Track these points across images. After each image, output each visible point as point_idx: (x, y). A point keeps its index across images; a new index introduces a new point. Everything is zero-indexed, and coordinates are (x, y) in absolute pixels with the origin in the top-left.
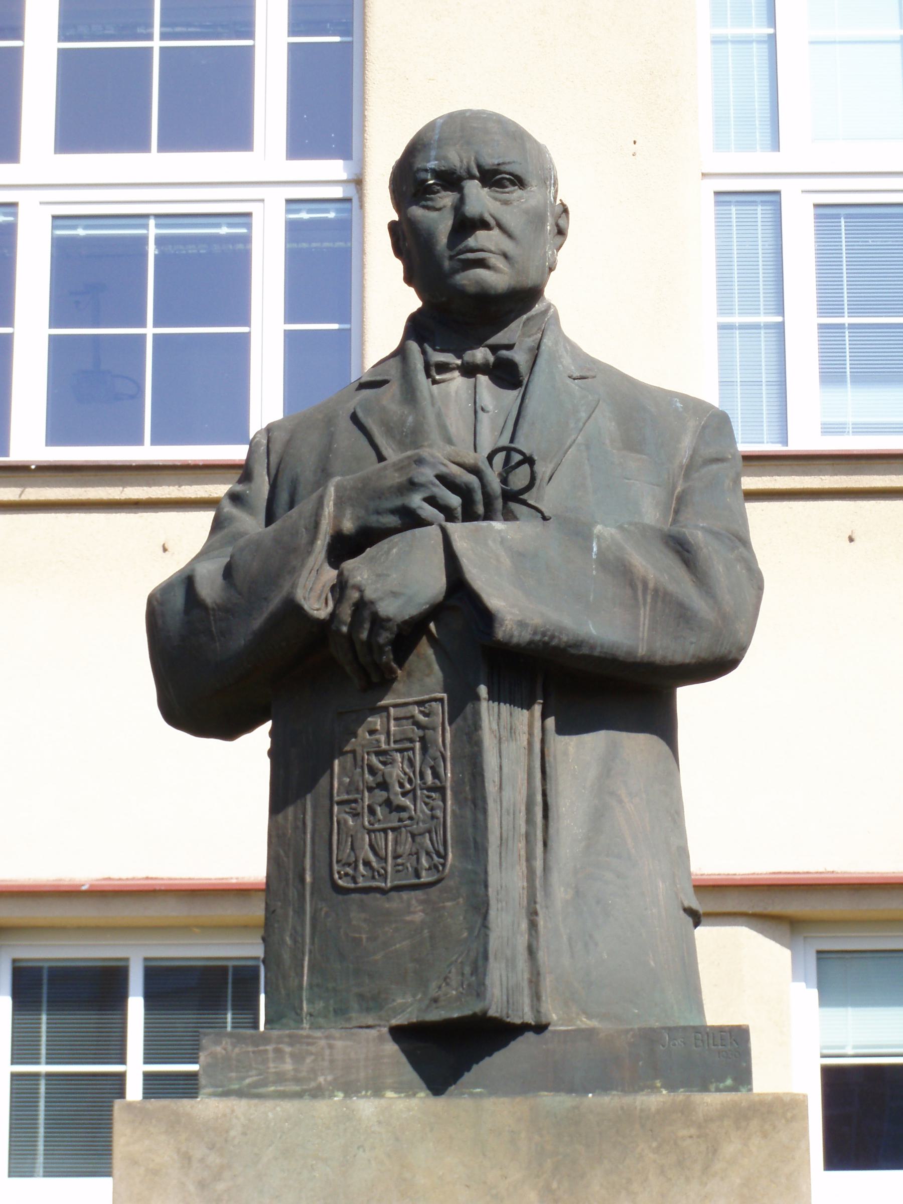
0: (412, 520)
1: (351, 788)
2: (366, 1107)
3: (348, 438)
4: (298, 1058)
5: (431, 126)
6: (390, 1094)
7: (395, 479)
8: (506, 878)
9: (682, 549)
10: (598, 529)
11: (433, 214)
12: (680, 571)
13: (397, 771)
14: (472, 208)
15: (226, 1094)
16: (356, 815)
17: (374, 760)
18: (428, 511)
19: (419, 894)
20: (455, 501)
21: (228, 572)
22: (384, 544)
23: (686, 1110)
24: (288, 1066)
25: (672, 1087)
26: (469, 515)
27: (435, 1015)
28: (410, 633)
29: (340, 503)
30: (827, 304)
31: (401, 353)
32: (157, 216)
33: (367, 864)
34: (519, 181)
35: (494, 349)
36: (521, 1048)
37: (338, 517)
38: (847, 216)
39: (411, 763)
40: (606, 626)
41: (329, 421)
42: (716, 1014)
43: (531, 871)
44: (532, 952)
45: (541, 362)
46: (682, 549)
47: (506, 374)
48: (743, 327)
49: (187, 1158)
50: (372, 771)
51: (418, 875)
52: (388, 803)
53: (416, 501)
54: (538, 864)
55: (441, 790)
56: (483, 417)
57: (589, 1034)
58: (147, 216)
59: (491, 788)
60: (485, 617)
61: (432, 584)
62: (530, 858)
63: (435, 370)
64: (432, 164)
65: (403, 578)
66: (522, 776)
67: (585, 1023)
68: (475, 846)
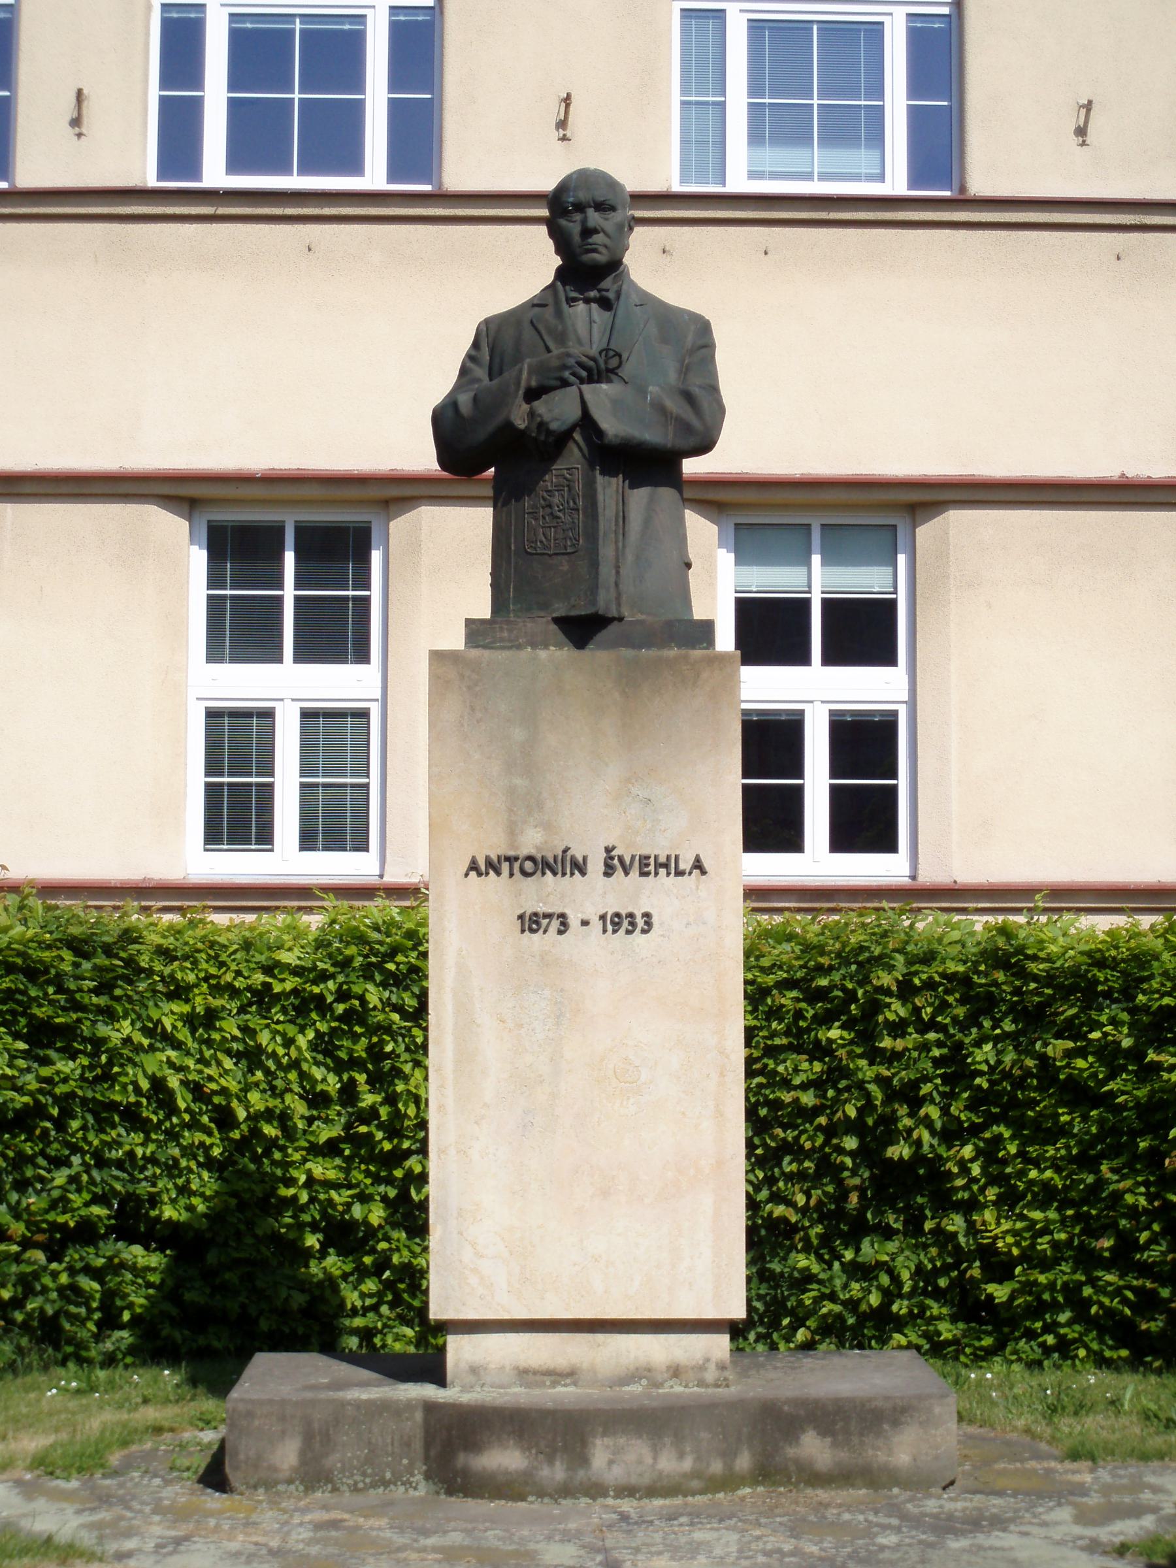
0: (565, 384)
1: (534, 506)
2: (543, 654)
3: (528, 334)
4: (510, 631)
5: (569, 177)
6: (552, 648)
7: (555, 363)
8: (607, 552)
9: (689, 397)
10: (651, 388)
11: (571, 224)
12: (688, 408)
13: (556, 500)
14: (591, 223)
15: (477, 647)
16: (536, 519)
17: (545, 494)
18: (572, 379)
19: (566, 557)
20: (584, 374)
21: (475, 399)
22: (551, 395)
23: (686, 658)
24: (505, 634)
25: (679, 647)
26: (590, 380)
27: (573, 613)
28: (564, 437)
29: (529, 373)
30: (755, 88)
31: (551, 287)
32: (301, 16)
33: (541, 542)
34: (613, 209)
35: (599, 291)
36: (613, 628)
37: (529, 379)
38: (770, 28)
39: (563, 496)
40: (653, 435)
41: (519, 323)
42: (699, 614)
43: (617, 549)
44: (617, 585)
45: (622, 298)
46: (689, 397)
47: (606, 304)
48: (697, 103)
49: (462, 676)
50: (544, 499)
51: (565, 548)
52: (552, 514)
53: (567, 374)
54: (620, 544)
55: (578, 510)
56: (595, 326)
57: (642, 622)
58: (294, 16)
59: (600, 510)
60: (600, 433)
61: (575, 414)
62: (616, 542)
63: (571, 301)
64: (571, 200)
65: (560, 409)
66: (614, 503)
67: (640, 617)
68: (593, 537)
